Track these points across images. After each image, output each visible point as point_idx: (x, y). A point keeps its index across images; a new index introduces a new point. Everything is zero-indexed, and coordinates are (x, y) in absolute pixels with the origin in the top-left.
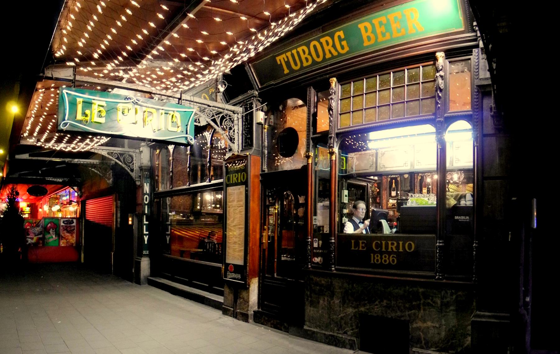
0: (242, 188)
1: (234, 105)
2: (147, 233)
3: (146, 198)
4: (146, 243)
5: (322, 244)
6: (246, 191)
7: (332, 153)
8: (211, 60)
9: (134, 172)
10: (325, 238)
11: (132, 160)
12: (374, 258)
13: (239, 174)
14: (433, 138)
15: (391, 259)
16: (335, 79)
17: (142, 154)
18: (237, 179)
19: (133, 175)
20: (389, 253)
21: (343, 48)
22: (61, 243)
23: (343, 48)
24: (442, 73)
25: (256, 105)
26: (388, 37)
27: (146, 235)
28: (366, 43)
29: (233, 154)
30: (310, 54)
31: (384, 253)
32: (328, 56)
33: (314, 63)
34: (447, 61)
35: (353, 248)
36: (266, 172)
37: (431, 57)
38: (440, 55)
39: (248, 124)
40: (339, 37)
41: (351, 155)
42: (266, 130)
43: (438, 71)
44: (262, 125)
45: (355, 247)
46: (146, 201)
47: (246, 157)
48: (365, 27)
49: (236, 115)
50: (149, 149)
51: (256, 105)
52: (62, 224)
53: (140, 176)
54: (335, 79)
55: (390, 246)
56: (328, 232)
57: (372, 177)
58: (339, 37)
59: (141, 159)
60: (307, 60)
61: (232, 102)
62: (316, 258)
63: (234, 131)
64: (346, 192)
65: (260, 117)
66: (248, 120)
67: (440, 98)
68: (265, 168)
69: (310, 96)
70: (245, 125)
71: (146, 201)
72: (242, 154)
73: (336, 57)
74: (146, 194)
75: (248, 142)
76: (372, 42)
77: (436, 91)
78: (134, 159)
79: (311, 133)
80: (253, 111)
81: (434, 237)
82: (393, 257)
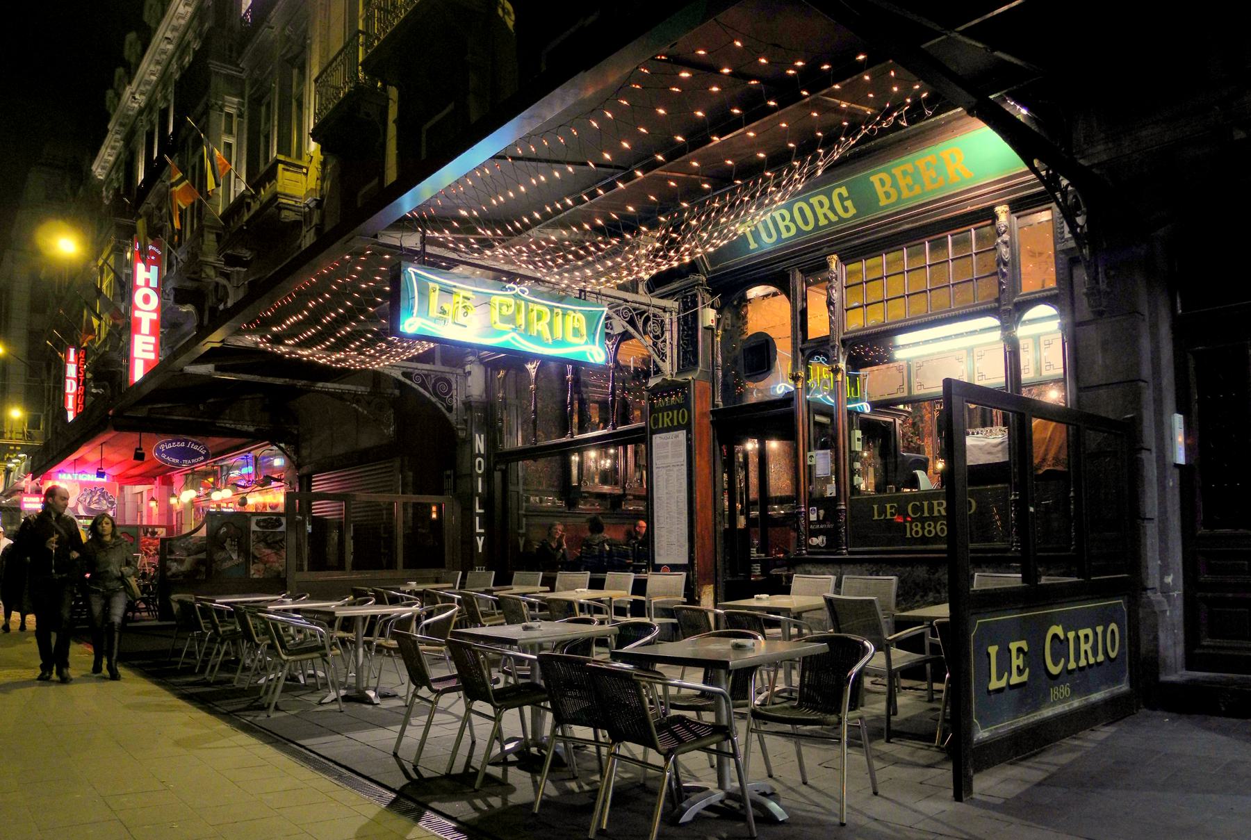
0: (682, 435)
1: (662, 298)
2: (482, 531)
3: (480, 462)
4: (480, 551)
5: (825, 515)
6: (688, 440)
7: (836, 371)
8: (642, 576)
9: (454, 412)
10: (828, 504)
11: (450, 389)
12: (911, 529)
13: (675, 412)
14: (997, 335)
15: (938, 528)
16: (835, 257)
17: (469, 378)
18: (672, 420)
19: (452, 417)
20: (935, 520)
21: (846, 210)
22: (252, 572)
23: (846, 210)
24: (1006, 237)
25: (702, 296)
26: (917, 190)
27: (480, 535)
28: (883, 202)
29: (664, 380)
30: (793, 220)
31: (926, 519)
32: (823, 222)
33: (800, 232)
34: (1014, 217)
35: (876, 517)
36: (721, 407)
37: (988, 214)
38: (1002, 211)
39: (689, 329)
40: (840, 195)
41: (862, 372)
42: (719, 339)
43: (999, 235)
44: (712, 329)
45: (879, 515)
46: (480, 469)
47: (687, 384)
48: (881, 180)
49: (668, 315)
50: (482, 367)
51: (702, 296)
52: (254, 527)
53: (466, 421)
54: (835, 257)
55: (936, 508)
56: (834, 495)
57: (901, 407)
58: (840, 195)
59: (466, 387)
60: (788, 229)
61: (657, 292)
62: (814, 539)
63: (665, 341)
64: (858, 434)
65: (709, 316)
66: (689, 325)
67: (1004, 275)
68: (719, 401)
69: (794, 283)
70: (683, 330)
71: (480, 469)
72: (680, 379)
73: (836, 223)
74: (479, 455)
75: (688, 357)
76: (893, 199)
77: (998, 265)
78: (454, 386)
79: (799, 341)
80: (697, 312)
81: (1006, 488)
82: (942, 524)
